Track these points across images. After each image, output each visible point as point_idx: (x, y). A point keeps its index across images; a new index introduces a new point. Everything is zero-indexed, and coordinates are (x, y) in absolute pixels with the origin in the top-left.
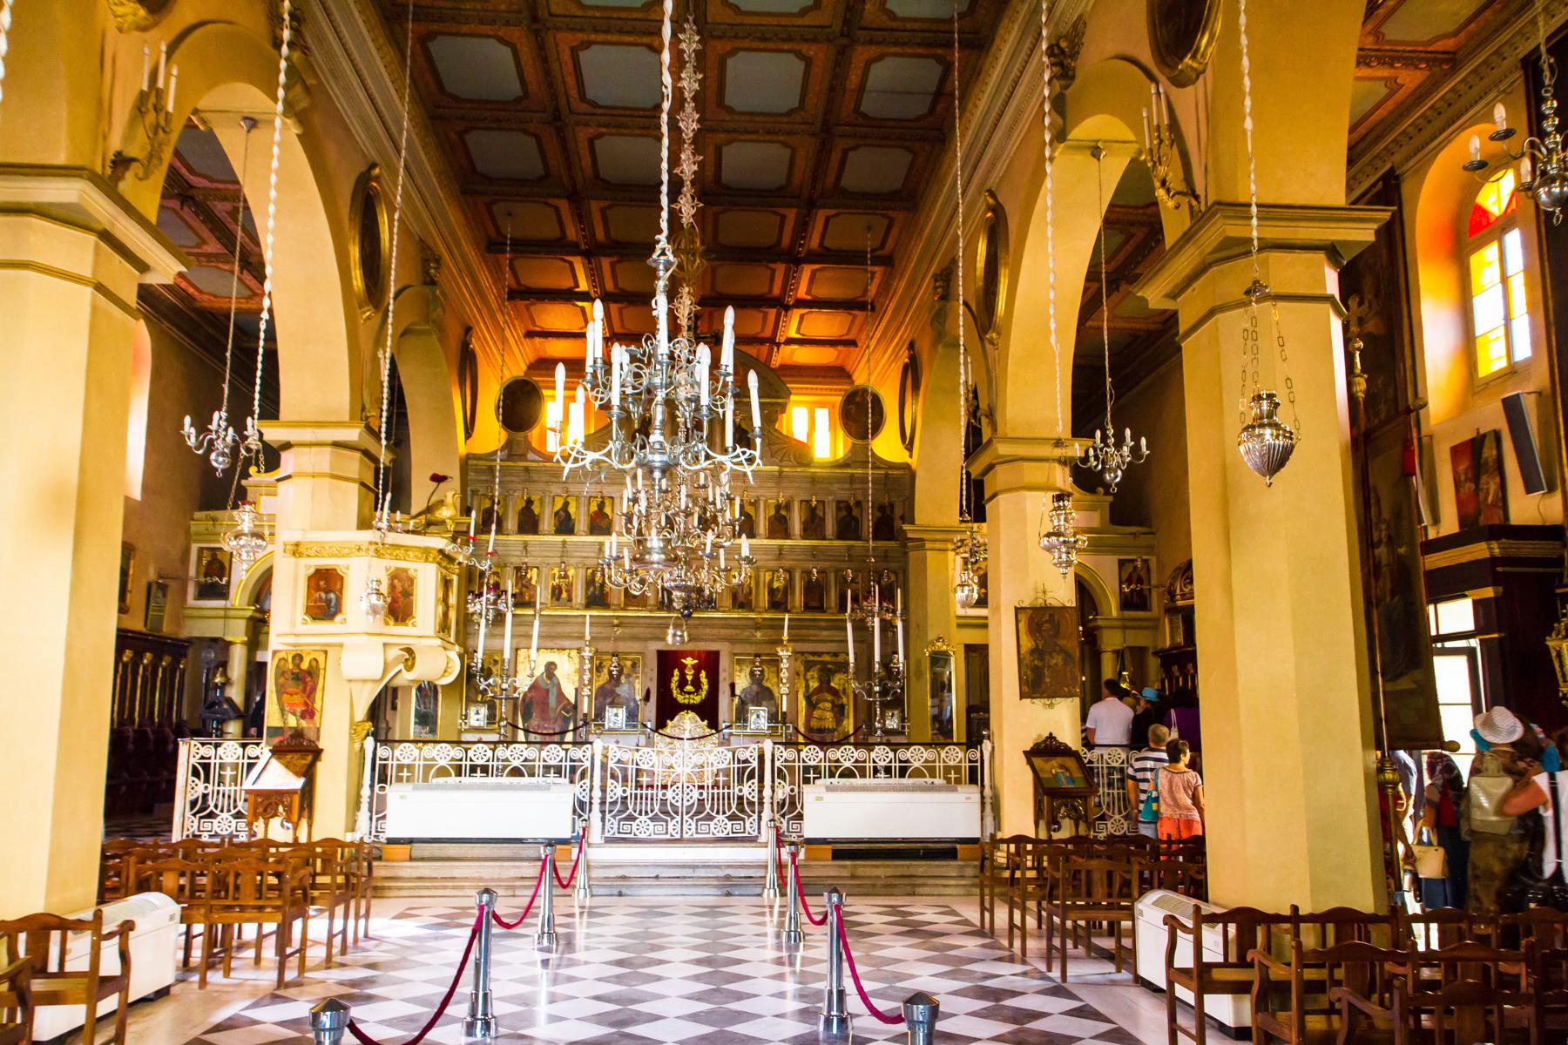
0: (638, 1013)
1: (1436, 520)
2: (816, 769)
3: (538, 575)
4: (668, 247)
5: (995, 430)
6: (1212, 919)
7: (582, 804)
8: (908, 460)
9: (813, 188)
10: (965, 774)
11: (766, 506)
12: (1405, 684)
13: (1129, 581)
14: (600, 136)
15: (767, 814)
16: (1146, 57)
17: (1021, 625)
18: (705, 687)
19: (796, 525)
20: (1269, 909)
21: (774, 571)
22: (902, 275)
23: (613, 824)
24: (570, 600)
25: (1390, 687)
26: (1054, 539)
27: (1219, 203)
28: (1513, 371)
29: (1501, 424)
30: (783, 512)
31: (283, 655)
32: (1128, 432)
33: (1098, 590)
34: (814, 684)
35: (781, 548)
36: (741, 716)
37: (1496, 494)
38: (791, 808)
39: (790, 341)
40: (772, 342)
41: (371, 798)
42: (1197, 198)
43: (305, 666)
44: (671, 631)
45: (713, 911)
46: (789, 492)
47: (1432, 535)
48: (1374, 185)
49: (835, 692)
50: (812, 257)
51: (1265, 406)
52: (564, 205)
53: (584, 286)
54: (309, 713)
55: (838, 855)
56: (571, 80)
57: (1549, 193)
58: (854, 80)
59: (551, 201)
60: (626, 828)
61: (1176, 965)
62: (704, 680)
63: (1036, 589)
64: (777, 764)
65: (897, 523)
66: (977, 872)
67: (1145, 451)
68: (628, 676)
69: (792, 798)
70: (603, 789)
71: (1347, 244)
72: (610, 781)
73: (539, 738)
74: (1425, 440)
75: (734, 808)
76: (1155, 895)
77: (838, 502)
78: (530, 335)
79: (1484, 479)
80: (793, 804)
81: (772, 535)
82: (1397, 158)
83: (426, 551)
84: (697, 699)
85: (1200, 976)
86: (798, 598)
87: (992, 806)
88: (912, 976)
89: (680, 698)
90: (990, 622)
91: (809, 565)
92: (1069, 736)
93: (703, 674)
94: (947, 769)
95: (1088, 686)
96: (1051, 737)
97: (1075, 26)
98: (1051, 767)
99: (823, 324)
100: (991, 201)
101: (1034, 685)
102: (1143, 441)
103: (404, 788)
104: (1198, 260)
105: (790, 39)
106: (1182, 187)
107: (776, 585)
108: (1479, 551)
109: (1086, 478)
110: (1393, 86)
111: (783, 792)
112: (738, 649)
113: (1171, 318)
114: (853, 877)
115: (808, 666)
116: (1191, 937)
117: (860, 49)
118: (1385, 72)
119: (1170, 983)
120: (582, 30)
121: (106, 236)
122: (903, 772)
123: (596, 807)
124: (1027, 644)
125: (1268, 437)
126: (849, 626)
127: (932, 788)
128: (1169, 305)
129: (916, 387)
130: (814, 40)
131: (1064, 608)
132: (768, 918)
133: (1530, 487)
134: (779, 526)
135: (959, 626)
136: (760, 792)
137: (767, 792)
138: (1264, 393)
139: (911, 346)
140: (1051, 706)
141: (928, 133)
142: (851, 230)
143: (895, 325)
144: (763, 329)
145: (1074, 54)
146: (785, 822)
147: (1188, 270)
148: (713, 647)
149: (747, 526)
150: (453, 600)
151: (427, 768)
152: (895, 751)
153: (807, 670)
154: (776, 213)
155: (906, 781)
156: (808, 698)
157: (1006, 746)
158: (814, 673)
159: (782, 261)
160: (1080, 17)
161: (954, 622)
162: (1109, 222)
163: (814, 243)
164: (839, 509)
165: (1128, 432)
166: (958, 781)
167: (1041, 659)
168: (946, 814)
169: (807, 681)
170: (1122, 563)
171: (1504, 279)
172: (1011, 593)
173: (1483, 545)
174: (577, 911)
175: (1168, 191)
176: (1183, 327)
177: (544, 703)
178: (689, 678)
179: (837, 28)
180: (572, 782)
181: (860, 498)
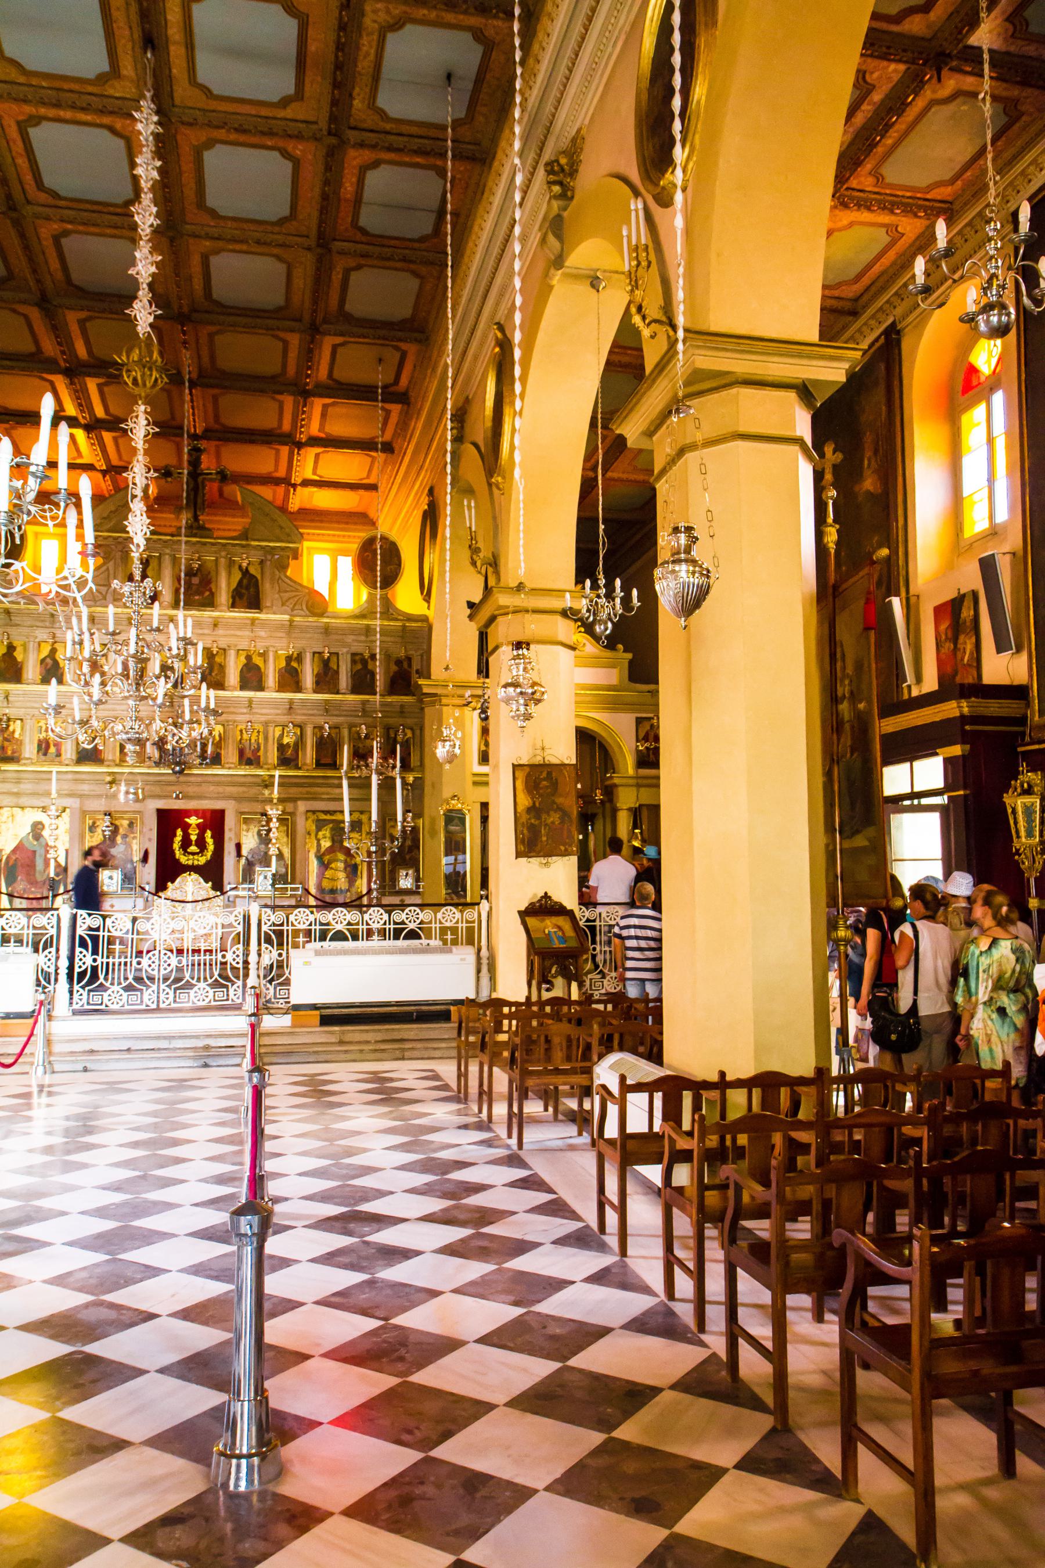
0: (39, 1209)
1: (919, 679)
3: (22, 728)
5: (498, 580)
7: (47, 977)
8: (426, 612)
9: (315, 311)
10: (462, 934)
11: (277, 657)
12: (860, 841)
14: (66, 233)
16: (635, 176)
19: (308, 679)
21: (284, 726)
22: (419, 414)
24: (59, 755)
25: (847, 844)
26: (511, 690)
28: (994, 532)
29: (978, 585)
30: (294, 664)
32: (618, 582)
33: (616, 749)
34: (326, 844)
35: (291, 702)
36: (248, 875)
37: (971, 653)
38: (278, 974)
39: (306, 483)
40: (286, 482)
44: (123, 788)
45: (181, 1084)
46: (300, 644)
47: (915, 693)
48: (877, 340)
49: (347, 852)
51: (683, 539)
52: (35, 314)
55: (326, 1020)
56: (22, 162)
57: (987, 322)
58: (348, 188)
59: (17, 307)
60: (97, 999)
63: (534, 745)
64: (264, 928)
65: (414, 676)
66: (455, 1034)
67: (635, 602)
68: (125, 836)
70: (71, 958)
71: (817, 382)
72: (78, 949)
73: (24, 904)
74: (913, 600)
77: (353, 655)
79: (962, 638)
81: (282, 687)
82: (899, 311)
84: (202, 860)
85: (623, 1146)
86: (309, 755)
87: (487, 966)
88: (365, 1150)
89: (184, 860)
90: (491, 780)
91: (320, 720)
92: (568, 898)
93: (209, 834)
94: (443, 930)
96: (546, 896)
97: (574, 140)
98: (549, 925)
100: (499, 335)
101: (530, 844)
105: (271, 134)
106: (658, 315)
107: (286, 740)
108: (951, 709)
110: (895, 234)
111: (271, 955)
112: (246, 807)
114: (341, 1042)
115: (320, 825)
117: (352, 153)
118: (886, 218)
120: (25, 101)
122: (397, 934)
124: (524, 801)
125: (683, 574)
126: (345, 783)
127: (427, 950)
128: (644, 444)
129: (434, 535)
130: (299, 137)
133: (1001, 646)
134: (290, 679)
135: (475, 783)
136: (246, 954)
137: (253, 958)
138: (682, 525)
139: (431, 492)
140: (547, 864)
141: (429, 254)
142: (359, 362)
144: (276, 470)
145: (573, 173)
146: (272, 988)
148: (217, 805)
149: (252, 678)
152: (389, 913)
153: (319, 829)
156: (320, 857)
157: (501, 904)
158: (326, 832)
159: (293, 394)
160: (579, 131)
161: (470, 779)
163: (323, 374)
164: (354, 662)
165: (618, 582)
166: (455, 942)
167: (538, 818)
168: (439, 975)
169: (318, 840)
170: (639, 721)
171: (990, 441)
172: (513, 747)
173: (953, 704)
174: (35, 1090)
175: (644, 318)
177: (31, 866)
178: (194, 838)
179: (323, 125)
180: (36, 951)
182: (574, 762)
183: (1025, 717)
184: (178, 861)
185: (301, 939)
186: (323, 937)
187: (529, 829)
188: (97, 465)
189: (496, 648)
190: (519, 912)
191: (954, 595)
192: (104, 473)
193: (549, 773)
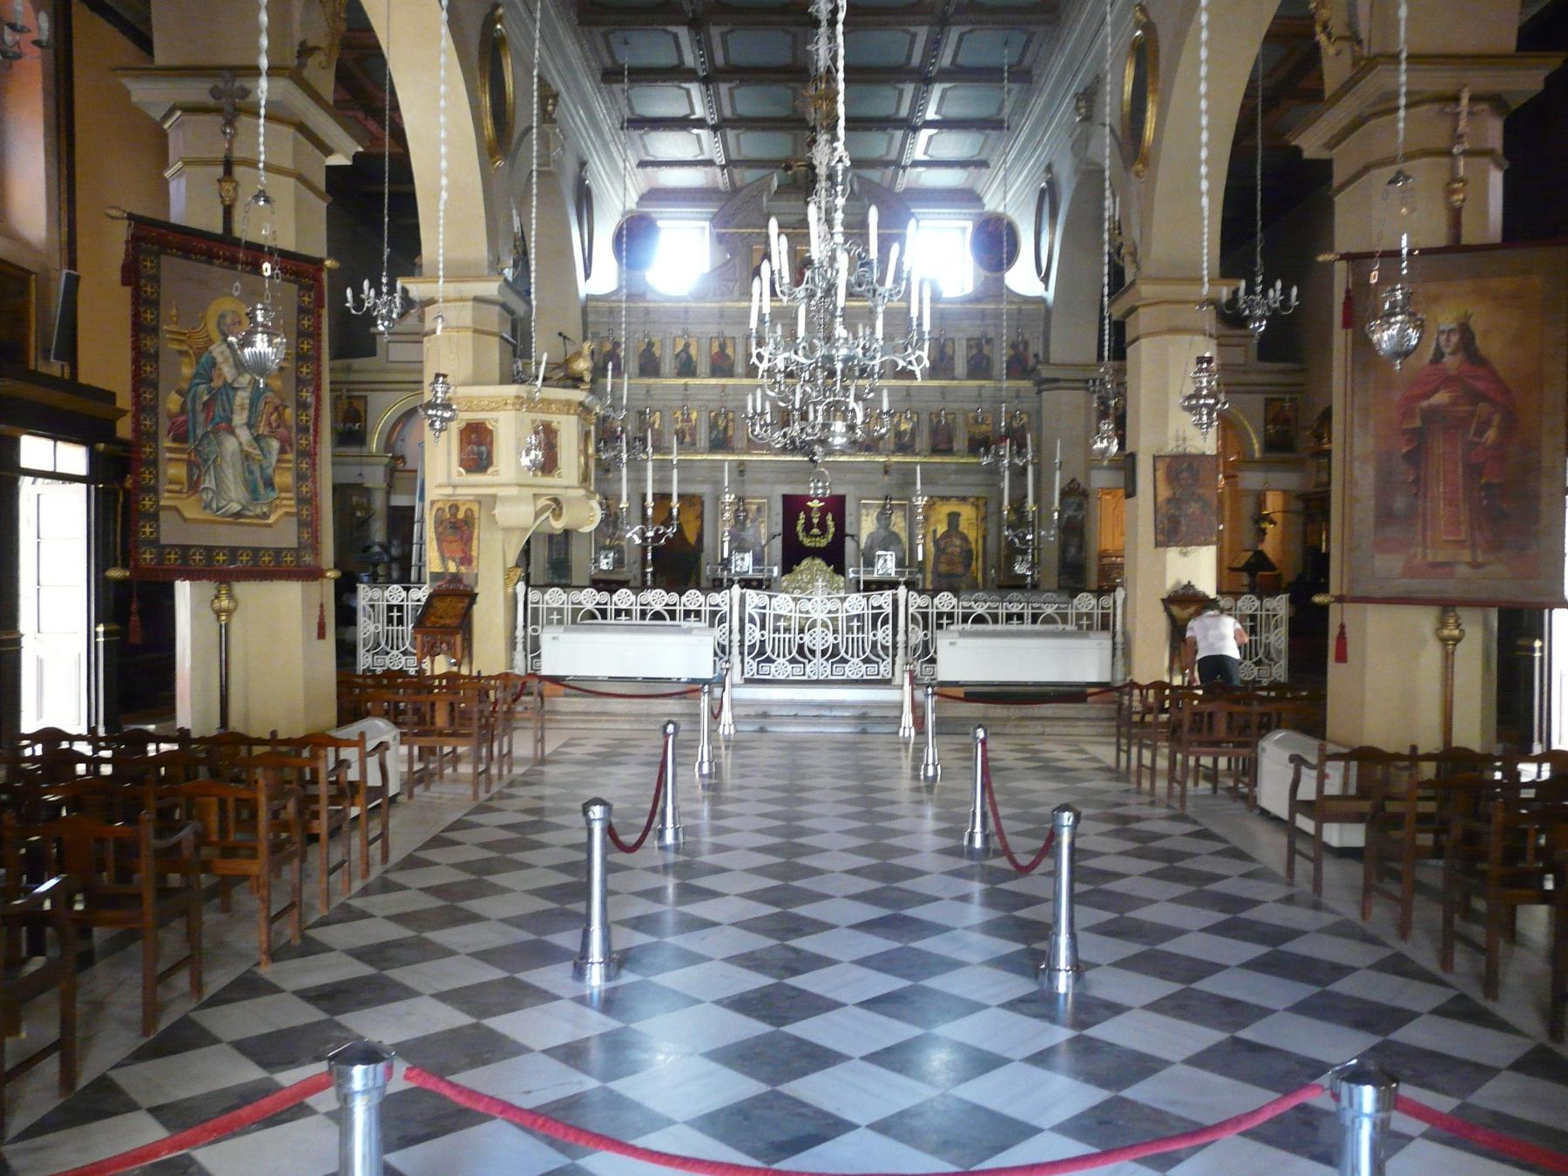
0: (802, 828)
2: (950, 616)
3: (661, 418)
4: (845, 154)
6: (1336, 757)
10: (1097, 620)
13: (1275, 421)
15: (900, 660)
17: (1159, 474)
18: (832, 530)
23: (751, 666)
24: (693, 444)
27: (1380, 55)
31: (439, 505)
39: (916, 164)
40: (897, 164)
41: (525, 637)
42: (1360, 42)
43: (461, 515)
50: (945, 75)
52: (683, 33)
53: (699, 112)
54: (467, 560)
61: (1300, 796)
62: (830, 523)
64: (911, 610)
69: (926, 643)
70: (742, 630)
75: (868, 651)
76: (1279, 735)
78: (643, 164)
80: (926, 651)
83: (568, 403)
87: (1123, 651)
89: (807, 542)
93: (830, 517)
94: (1079, 616)
95: (1226, 536)
96: (1189, 586)
99: (953, 145)
102: (1295, 291)
103: (557, 631)
107: (904, 427)
109: (1231, 317)
111: (918, 635)
113: (1325, 167)
116: (1314, 773)
119: (1292, 814)
121: (302, 128)
123: (736, 650)
128: (1325, 155)
131: (1203, 456)
132: (903, 754)
136: (895, 633)
137: (901, 637)
140: (1185, 554)
143: (1033, 144)
144: (888, 152)
150: (591, 450)
151: (575, 612)
154: (907, 32)
155: (1038, 627)
159: (911, 81)
162: (1271, 37)
164: (969, 347)
166: (1090, 627)
168: (1084, 661)
170: (1268, 402)
175: (1329, 36)
176: (1337, 179)
178: (816, 521)
180: (712, 625)
181: (991, 335)
184: (801, 543)
185: (945, 621)
186: (965, 619)
188: (718, 161)
189: (1136, 340)
192: (723, 167)
193: (1190, 465)
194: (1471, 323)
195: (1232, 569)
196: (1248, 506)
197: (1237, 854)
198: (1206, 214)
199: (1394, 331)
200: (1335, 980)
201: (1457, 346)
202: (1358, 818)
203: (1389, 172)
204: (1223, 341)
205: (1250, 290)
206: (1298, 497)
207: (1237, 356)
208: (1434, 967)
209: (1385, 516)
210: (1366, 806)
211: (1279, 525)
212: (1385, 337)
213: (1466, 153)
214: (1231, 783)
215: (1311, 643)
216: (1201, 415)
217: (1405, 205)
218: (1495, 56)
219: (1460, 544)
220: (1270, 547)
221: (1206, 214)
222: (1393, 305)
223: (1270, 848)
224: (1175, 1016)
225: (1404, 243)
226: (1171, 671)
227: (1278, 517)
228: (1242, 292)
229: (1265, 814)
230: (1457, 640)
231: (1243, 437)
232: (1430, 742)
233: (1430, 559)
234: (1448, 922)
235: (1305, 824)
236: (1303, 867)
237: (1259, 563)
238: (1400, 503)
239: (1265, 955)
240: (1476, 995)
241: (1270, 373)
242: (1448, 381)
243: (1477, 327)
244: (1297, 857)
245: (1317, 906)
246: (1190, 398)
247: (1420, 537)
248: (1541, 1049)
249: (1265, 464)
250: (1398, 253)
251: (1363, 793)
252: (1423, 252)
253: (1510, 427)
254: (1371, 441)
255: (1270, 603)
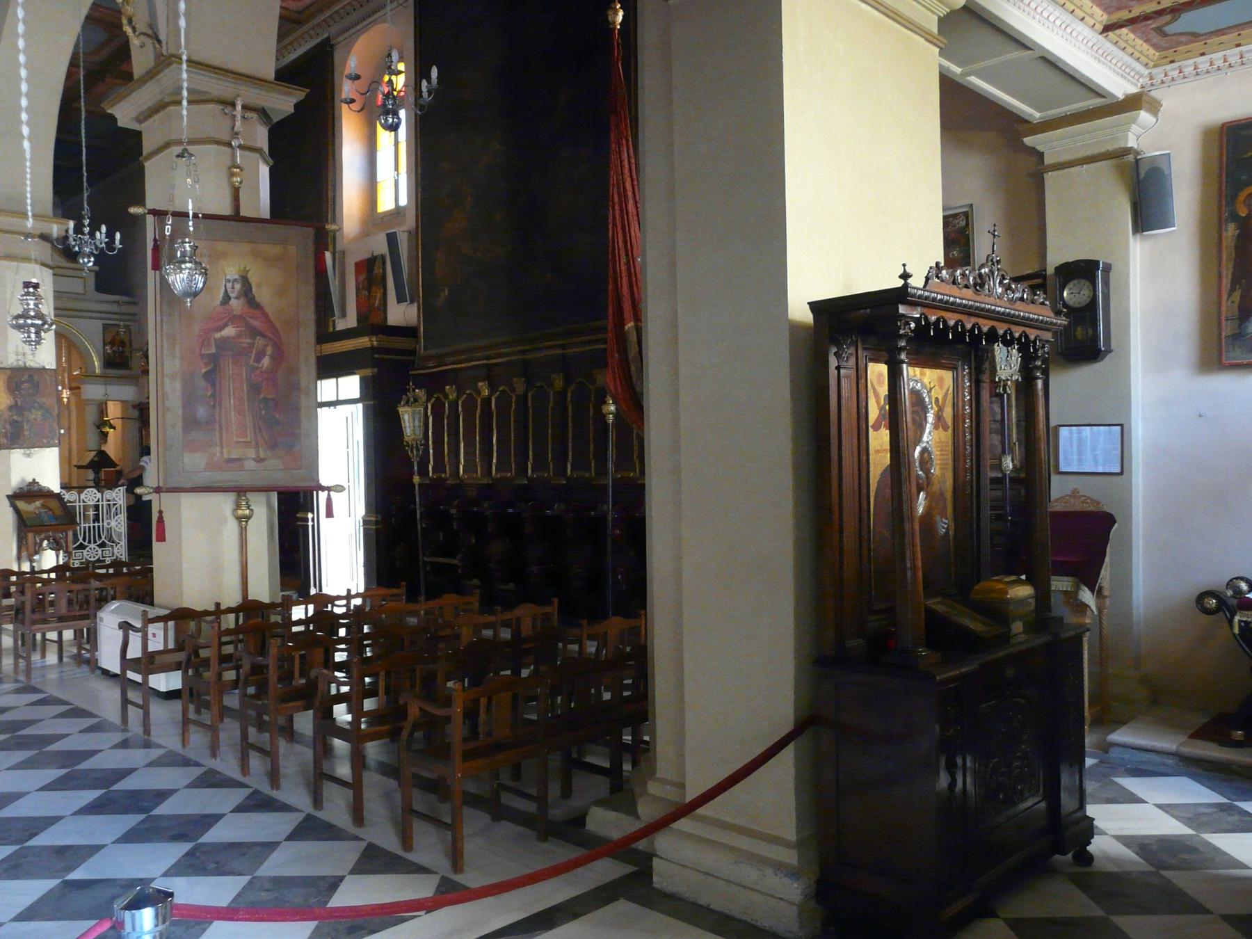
1: (344, 315)
13: (112, 343)
20: (199, 608)
28: (398, 212)
42: (159, 42)
61: (128, 657)
76: (114, 605)
79: (373, 289)
96: (34, 482)
102: (118, 236)
104: (159, 97)
108: (364, 342)
119: (124, 670)
128: (134, 126)
131: (44, 369)
133: (400, 299)
140: (29, 455)
147: (150, 104)
167: (21, 415)
170: (105, 327)
175: (134, 30)
176: (147, 147)
182: (54, 367)
183: (415, 351)
187: (11, 424)
190: (8, 496)
191: (368, 256)
193: (31, 376)
194: (249, 276)
195: (79, 467)
196: (91, 414)
197: (78, 713)
198: (28, 156)
199: (185, 275)
200: (157, 804)
201: (240, 292)
202: (177, 666)
203: (177, 150)
204: (58, 271)
205: (78, 229)
206: (134, 407)
207: (75, 286)
208: (238, 776)
209: (191, 423)
210: (181, 656)
211: (119, 427)
212: (179, 279)
213: (241, 147)
214: (75, 651)
215: (143, 527)
216: (29, 332)
217: (189, 177)
218: (254, 78)
219: (247, 444)
220: (112, 448)
221: (28, 156)
222: (184, 254)
223: (107, 700)
224: (9, 878)
225: (190, 207)
226: (19, 558)
227: (118, 423)
228: (71, 231)
229: (106, 673)
230: (248, 518)
231: (85, 358)
232: (232, 598)
233: (226, 456)
234: (244, 736)
235: (131, 675)
236: (134, 714)
237: (101, 461)
238: (202, 412)
239: (100, 797)
240: (266, 789)
241: (106, 303)
242: (234, 319)
243: (253, 279)
244: (130, 706)
245: (147, 745)
246: (18, 317)
247: (217, 439)
248: (309, 817)
249: (105, 379)
250: (187, 215)
251: (180, 647)
252: (206, 216)
253: (279, 356)
254: (177, 362)
255: (109, 494)
